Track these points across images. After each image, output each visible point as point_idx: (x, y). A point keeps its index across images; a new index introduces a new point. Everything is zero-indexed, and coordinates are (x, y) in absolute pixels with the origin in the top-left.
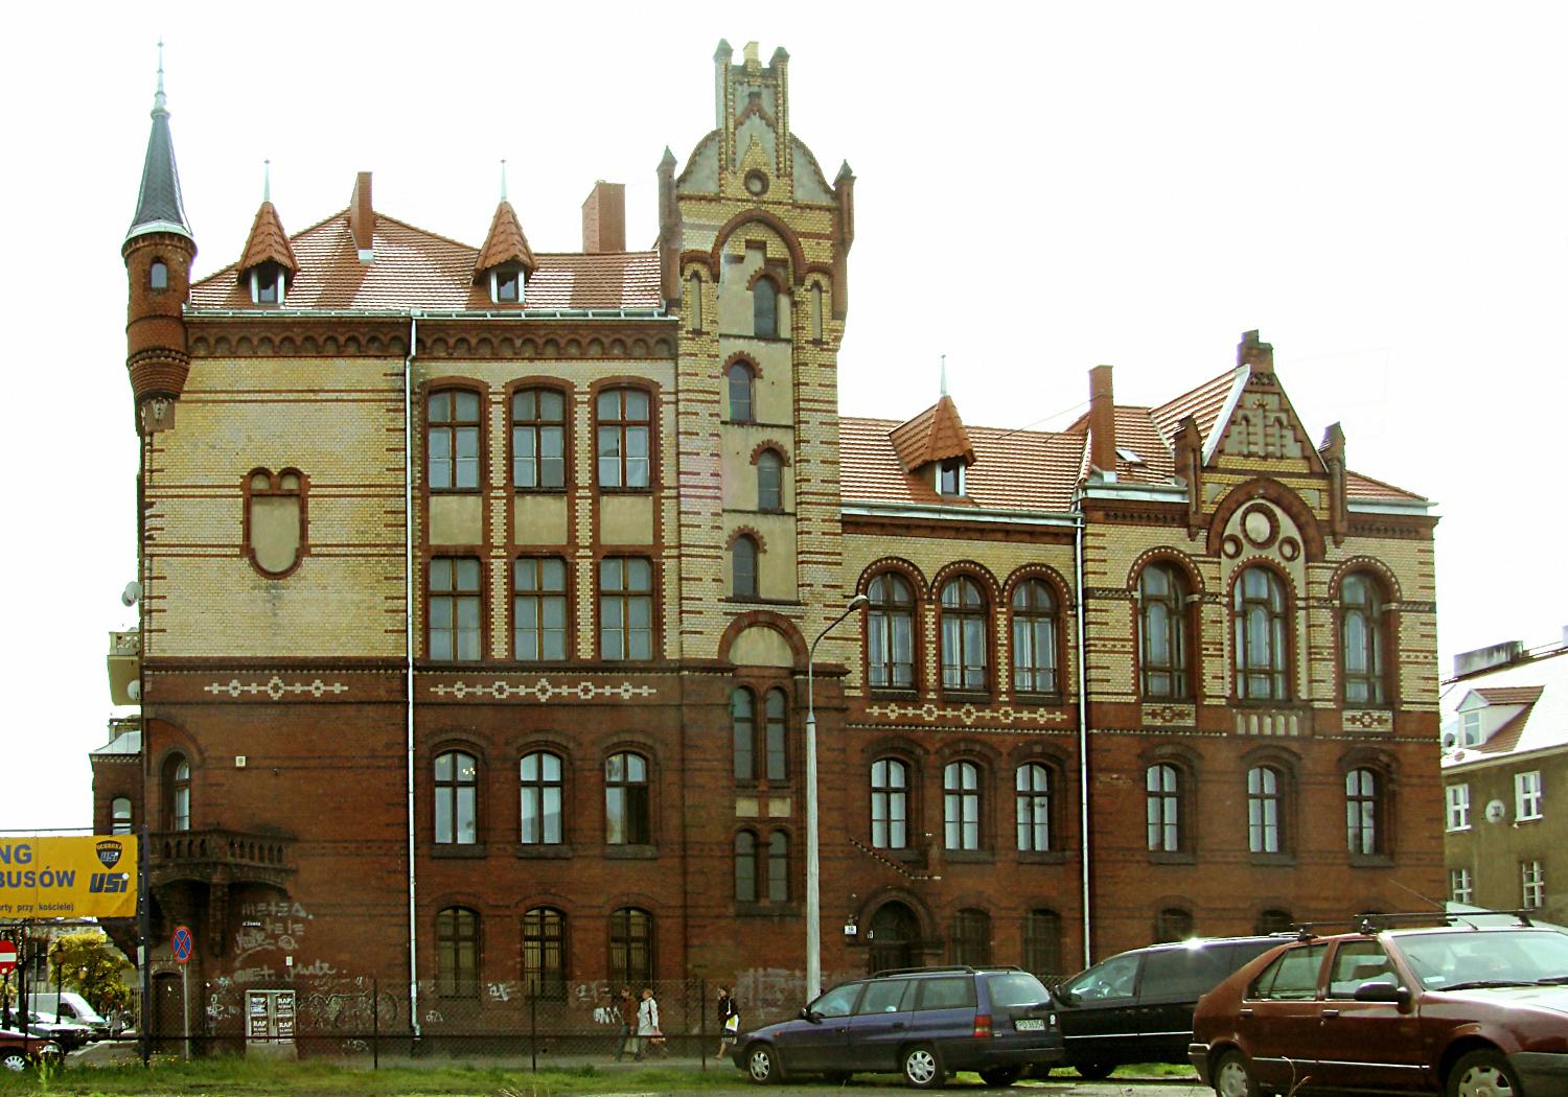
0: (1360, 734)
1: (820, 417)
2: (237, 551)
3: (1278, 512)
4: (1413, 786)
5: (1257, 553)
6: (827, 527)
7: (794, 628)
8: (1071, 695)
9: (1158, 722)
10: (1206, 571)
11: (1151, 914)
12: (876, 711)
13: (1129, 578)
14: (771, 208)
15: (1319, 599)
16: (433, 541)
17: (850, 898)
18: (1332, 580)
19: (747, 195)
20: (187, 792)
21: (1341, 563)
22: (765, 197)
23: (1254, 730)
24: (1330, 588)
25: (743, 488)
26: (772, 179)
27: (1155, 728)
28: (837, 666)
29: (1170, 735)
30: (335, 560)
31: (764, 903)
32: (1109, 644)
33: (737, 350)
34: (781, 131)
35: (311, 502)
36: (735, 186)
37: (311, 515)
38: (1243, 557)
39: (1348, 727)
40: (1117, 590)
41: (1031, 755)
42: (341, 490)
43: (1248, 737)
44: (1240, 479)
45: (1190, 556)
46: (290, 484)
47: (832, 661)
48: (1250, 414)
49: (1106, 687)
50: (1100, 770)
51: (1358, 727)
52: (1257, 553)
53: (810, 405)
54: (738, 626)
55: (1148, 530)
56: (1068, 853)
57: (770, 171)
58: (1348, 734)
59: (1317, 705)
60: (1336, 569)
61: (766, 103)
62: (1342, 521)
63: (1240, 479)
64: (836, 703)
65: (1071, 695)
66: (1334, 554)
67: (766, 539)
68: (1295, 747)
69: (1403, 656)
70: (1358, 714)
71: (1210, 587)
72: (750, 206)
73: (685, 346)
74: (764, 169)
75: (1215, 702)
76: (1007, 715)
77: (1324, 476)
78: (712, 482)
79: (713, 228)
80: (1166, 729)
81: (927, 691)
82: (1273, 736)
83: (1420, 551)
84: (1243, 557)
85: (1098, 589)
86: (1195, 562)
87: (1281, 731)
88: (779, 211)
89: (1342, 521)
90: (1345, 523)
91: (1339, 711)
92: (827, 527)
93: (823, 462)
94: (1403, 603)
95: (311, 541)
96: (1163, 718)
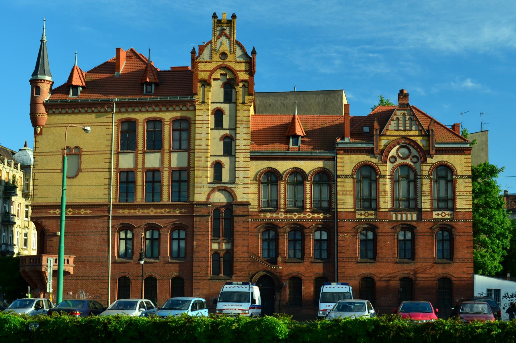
0: (440, 219)
1: (244, 126)
2: (60, 171)
3: (411, 148)
4: (460, 236)
5: (402, 161)
6: (245, 159)
7: (233, 191)
8: (333, 209)
9: (363, 217)
10: (381, 168)
11: (358, 278)
12: (262, 215)
13: (353, 171)
14: (229, 64)
15: (425, 176)
16: (120, 167)
17: (249, 274)
18: (430, 169)
19: (220, 60)
20: (120, 72)
21: (434, 164)
22: (226, 60)
23: (404, 219)
24: (429, 172)
25: (218, 148)
26: (229, 54)
27: (361, 219)
28: (247, 202)
29: (367, 221)
30: (101, 150)
31: (508, 248)
32: (345, 193)
33: (217, 107)
34: (232, 40)
35: (83, 157)
36: (216, 57)
37: (83, 160)
38: (397, 163)
39: (435, 217)
40: (348, 175)
41: (318, 228)
42: (92, 153)
43: (397, 221)
44: (395, 138)
45: (375, 163)
46: (76, 151)
47: (245, 200)
48: (399, 117)
49: (342, 206)
50: (340, 233)
51: (440, 217)
52: (402, 161)
53: (240, 122)
54: (213, 190)
55: (360, 156)
56: (331, 259)
57: (228, 52)
58: (436, 219)
59: (423, 210)
60: (431, 166)
61: (227, 32)
62: (432, 150)
63: (395, 138)
64: (246, 213)
65: (333, 209)
66: (429, 160)
67: (225, 164)
68: (414, 224)
69: (457, 193)
70: (440, 212)
71: (383, 173)
72: (221, 63)
73: (197, 107)
74: (226, 52)
75: (384, 210)
76: (309, 215)
77: (425, 135)
78: (206, 147)
79: (207, 71)
80: (366, 219)
81: (281, 208)
82: (407, 221)
83: (465, 158)
84: (397, 163)
85: (341, 175)
86: (377, 165)
87: (410, 219)
88: (230, 64)
89: (432, 150)
90: (434, 151)
91: (432, 211)
92: (245, 159)
93: (244, 140)
94: (458, 176)
95: (82, 167)
96: (365, 215)
